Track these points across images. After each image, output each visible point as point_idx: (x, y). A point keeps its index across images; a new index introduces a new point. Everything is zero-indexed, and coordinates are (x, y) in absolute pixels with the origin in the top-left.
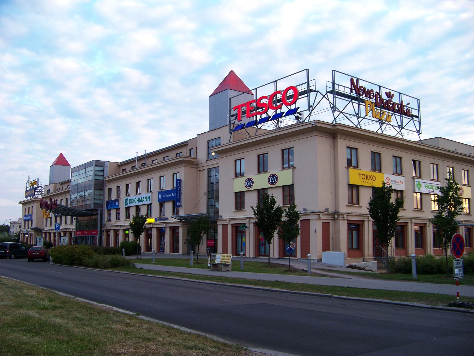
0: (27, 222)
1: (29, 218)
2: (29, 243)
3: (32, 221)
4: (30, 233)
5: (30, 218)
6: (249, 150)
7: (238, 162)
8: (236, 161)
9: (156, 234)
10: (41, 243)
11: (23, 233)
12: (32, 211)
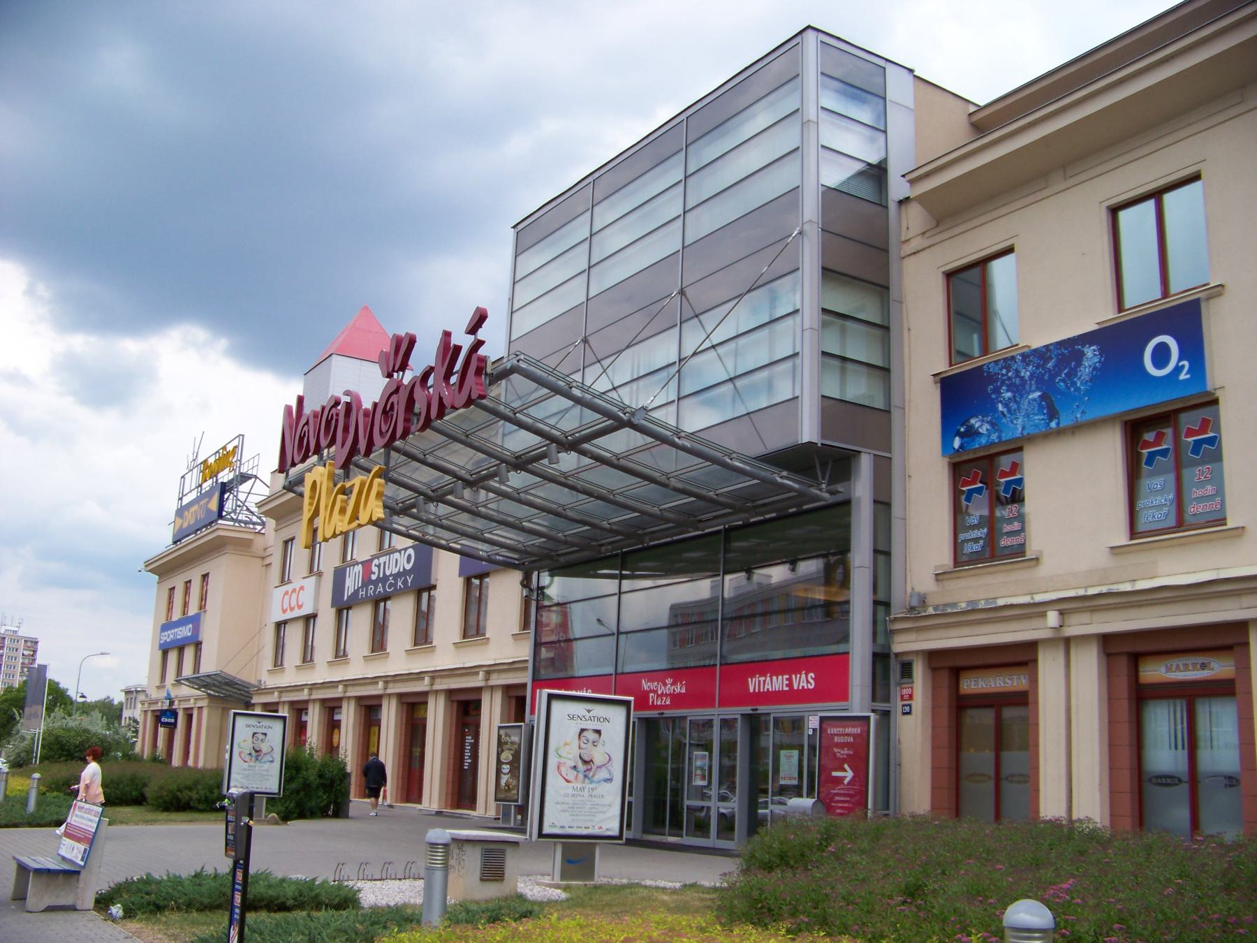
0: (173, 657)
1: (185, 632)
2: (176, 761)
3: (198, 645)
4: (186, 709)
5: (189, 634)
6: (949, 236)
7: (1137, 221)
8: (1114, 211)
9: (444, 725)
10: (267, 766)
11: (154, 707)
12: (203, 598)
